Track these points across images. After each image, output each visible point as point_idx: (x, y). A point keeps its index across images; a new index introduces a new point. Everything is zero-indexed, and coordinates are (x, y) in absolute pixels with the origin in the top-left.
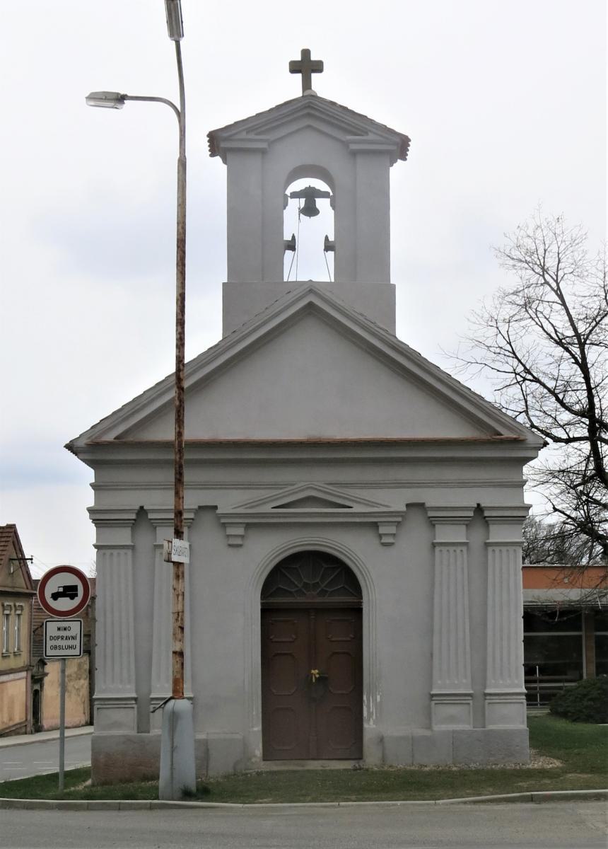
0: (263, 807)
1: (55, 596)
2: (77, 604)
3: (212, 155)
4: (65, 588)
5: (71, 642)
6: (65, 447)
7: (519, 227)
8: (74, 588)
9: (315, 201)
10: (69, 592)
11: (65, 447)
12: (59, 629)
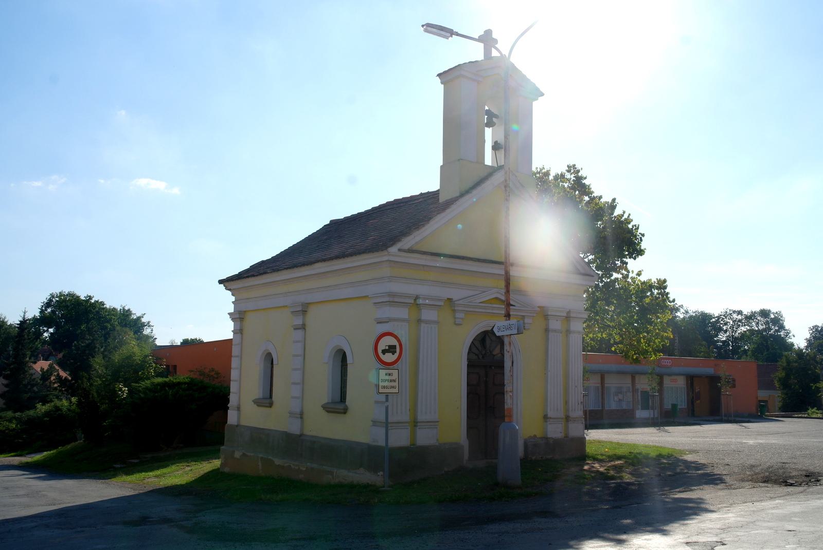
0: (685, 503)
1: (384, 352)
2: (396, 358)
3: (448, 39)
4: (389, 346)
5: (393, 384)
6: (253, 401)
7: (304, 310)
8: (394, 347)
9: (810, 343)
10: (391, 349)
11: (253, 401)
12: (386, 374)
